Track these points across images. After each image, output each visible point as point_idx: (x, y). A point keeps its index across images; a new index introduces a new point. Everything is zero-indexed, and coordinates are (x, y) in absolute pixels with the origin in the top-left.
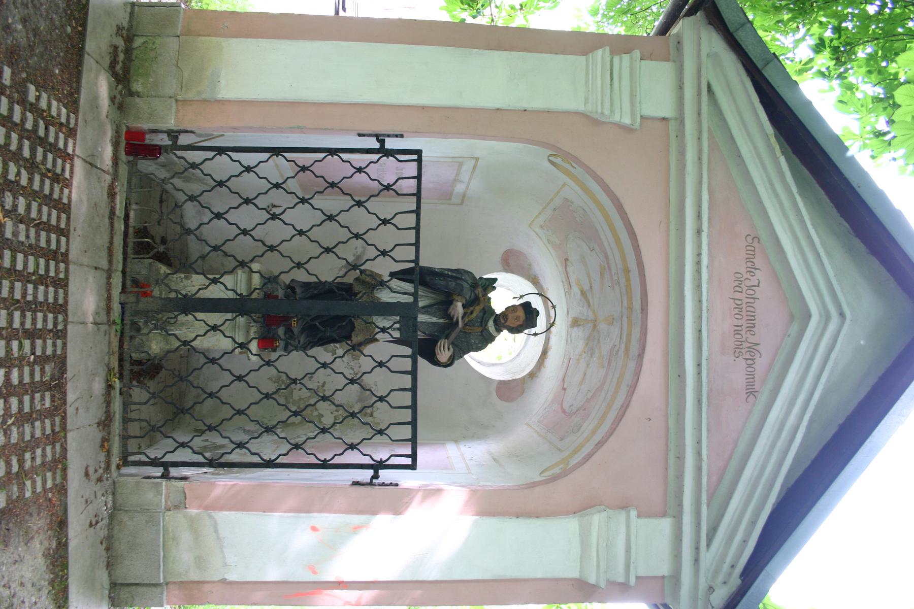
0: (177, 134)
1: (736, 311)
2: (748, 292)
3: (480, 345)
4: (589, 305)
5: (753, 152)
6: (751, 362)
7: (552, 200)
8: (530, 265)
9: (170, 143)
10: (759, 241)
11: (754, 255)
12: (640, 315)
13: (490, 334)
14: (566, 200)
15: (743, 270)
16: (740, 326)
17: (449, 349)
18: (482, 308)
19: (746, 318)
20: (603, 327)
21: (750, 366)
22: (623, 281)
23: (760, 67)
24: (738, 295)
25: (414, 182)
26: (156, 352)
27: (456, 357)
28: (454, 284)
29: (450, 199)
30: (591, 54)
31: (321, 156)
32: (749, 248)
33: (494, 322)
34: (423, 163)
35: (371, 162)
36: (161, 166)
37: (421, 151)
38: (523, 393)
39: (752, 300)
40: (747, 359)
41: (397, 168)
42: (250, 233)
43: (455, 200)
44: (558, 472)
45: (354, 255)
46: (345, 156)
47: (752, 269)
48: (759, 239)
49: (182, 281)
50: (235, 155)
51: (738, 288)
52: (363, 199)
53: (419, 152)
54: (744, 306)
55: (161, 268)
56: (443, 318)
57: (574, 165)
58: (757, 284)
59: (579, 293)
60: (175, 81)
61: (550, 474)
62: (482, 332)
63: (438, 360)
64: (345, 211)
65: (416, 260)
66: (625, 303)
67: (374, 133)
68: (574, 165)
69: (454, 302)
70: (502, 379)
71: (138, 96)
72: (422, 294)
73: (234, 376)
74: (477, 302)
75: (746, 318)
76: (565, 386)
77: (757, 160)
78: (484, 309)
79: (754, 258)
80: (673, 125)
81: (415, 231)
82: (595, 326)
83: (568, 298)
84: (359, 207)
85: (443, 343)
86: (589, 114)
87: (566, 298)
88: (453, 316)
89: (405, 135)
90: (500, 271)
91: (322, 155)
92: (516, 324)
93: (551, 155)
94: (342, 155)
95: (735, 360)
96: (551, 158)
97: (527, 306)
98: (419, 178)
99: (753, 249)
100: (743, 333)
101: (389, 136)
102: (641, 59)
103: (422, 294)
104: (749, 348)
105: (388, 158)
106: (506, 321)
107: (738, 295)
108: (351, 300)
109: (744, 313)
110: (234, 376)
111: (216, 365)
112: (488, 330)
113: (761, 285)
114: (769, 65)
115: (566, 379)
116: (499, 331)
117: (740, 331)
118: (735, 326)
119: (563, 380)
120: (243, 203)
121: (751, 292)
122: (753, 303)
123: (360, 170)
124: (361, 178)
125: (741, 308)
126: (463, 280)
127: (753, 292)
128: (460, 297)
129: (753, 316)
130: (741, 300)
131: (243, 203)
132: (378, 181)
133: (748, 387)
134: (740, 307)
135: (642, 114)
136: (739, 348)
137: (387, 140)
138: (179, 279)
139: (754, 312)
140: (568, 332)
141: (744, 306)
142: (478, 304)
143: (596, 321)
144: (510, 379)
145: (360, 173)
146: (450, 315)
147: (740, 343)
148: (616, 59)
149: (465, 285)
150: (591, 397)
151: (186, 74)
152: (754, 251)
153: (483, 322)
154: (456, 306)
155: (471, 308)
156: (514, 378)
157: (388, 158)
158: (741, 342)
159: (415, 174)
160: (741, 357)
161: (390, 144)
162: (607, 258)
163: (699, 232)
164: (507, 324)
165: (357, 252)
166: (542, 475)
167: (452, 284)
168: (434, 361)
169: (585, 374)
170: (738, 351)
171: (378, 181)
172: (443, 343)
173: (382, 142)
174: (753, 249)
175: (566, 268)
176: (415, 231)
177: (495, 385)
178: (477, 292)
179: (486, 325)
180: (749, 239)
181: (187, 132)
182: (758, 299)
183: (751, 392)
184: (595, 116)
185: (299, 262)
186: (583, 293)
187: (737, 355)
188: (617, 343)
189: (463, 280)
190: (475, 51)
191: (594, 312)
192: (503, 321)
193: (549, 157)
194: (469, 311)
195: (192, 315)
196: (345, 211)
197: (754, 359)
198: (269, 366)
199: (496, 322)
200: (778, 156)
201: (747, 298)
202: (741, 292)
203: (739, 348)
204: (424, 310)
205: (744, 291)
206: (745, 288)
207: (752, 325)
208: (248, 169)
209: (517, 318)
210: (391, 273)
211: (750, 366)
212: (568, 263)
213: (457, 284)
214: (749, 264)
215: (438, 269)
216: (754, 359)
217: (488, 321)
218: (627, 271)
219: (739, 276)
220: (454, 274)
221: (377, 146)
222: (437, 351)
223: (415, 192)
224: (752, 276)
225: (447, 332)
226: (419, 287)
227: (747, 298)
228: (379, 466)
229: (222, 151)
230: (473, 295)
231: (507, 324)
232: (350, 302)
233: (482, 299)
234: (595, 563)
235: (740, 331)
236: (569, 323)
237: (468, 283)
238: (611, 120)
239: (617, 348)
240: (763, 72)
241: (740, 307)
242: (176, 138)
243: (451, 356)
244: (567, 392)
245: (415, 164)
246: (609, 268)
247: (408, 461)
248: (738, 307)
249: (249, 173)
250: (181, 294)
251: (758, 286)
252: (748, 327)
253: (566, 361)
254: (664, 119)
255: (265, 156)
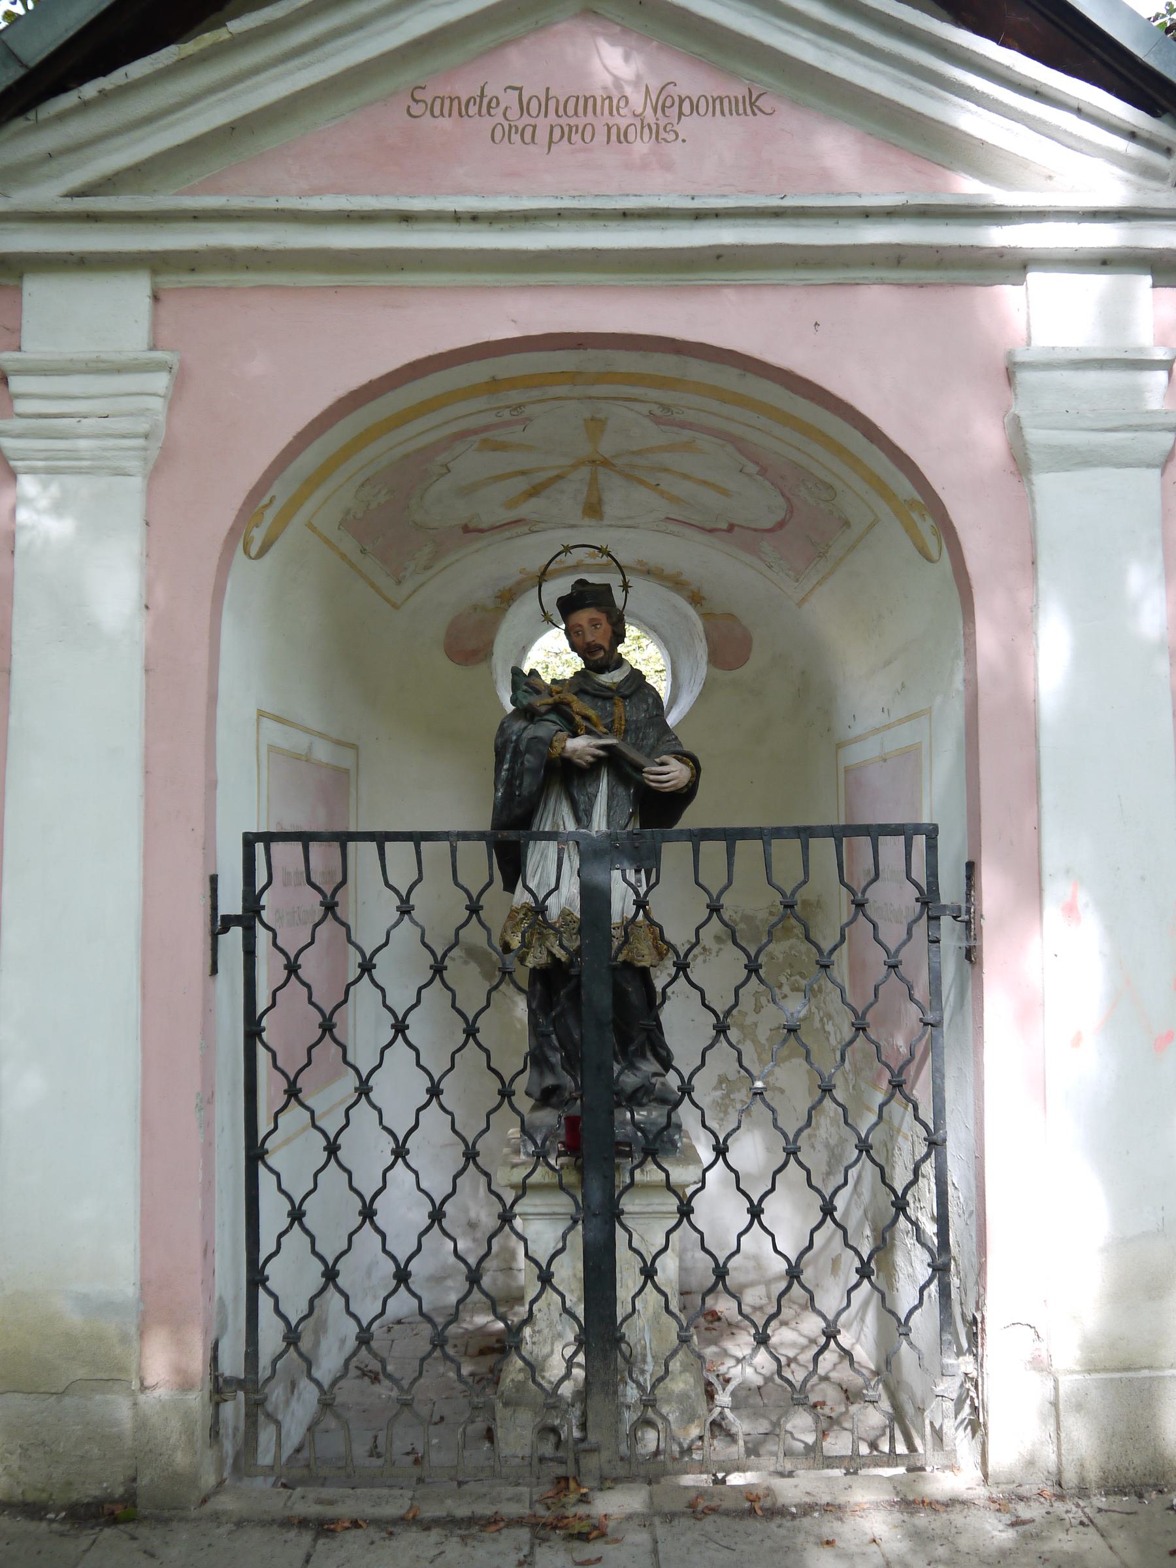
0: (221, 1380)
1: (576, 138)
2: (534, 112)
3: (650, 701)
4: (559, 477)
5: (221, 95)
6: (686, 105)
7: (343, 556)
8: (475, 608)
9: (241, 1395)
10: (421, 88)
11: (452, 100)
12: (591, 353)
13: (627, 679)
14: (343, 523)
15: (487, 123)
16: (609, 129)
17: (662, 764)
18: (575, 698)
19: (590, 117)
20: (607, 447)
21: (694, 108)
22: (515, 397)
23: (21, 72)
24: (542, 135)
25: (314, 847)
26: (692, 1380)
27: (678, 748)
28: (527, 756)
29: (347, 771)
30: (12, 463)
31: (262, 1055)
32: (437, 111)
33: (602, 672)
34: (273, 829)
35: (275, 944)
36: (292, 1392)
37: (246, 836)
38: (731, 616)
39: (552, 104)
40: (681, 114)
41: (285, 885)
42: (438, 1203)
43: (346, 760)
44: (930, 521)
45: (466, 963)
46: (262, 1002)
47: (484, 103)
48: (416, 88)
49: (539, 1332)
50: (267, 1246)
51: (528, 135)
52: (355, 958)
53: (249, 841)
54: (564, 121)
55: (513, 1380)
56: (598, 778)
57: (266, 500)
58: (517, 92)
59: (534, 500)
60: (98, 1397)
61: (934, 538)
62: (624, 697)
63: (687, 786)
64: (384, 997)
65: (480, 836)
66: (561, 390)
67: (209, 939)
68: (266, 500)
69: (567, 755)
70: (705, 658)
71: (134, 1480)
72: (549, 823)
73: (751, 1224)
74: (565, 708)
75: (590, 117)
76: (725, 526)
77: (240, 87)
78: (576, 694)
79: (458, 98)
80: (168, 281)
81: (423, 843)
82: (606, 463)
83: (542, 525)
84: (374, 966)
85: (652, 777)
86: (150, 466)
87: (544, 530)
88: (594, 756)
89: (212, 872)
90: (490, 667)
91: (261, 1051)
92: (605, 627)
93: (246, 551)
94: (260, 1008)
95: (684, 141)
96: (254, 550)
97: (568, 606)
98: (305, 838)
99: (438, 102)
100: (623, 123)
101: (214, 908)
102: (19, 349)
103: (549, 823)
104: (655, 111)
105: (263, 908)
106: (601, 648)
107: (542, 135)
108: (579, 976)
109: (580, 121)
110: (751, 1224)
111: (730, 1265)
112: (620, 685)
113: (518, 85)
114: (18, 50)
115: (709, 526)
116: (620, 662)
117: (619, 129)
118: (608, 141)
119: (711, 531)
120: (372, 1223)
121: (534, 104)
122: (558, 101)
123: (292, 968)
124: (309, 966)
125: (570, 128)
126: (519, 737)
127: (534, 101)
128: (556, 744)
129: (586, 100)
130: (552, 127)
131: (372, 1223)
132: (316, 926)
133: (741, 111)
134: (566, 130)
135: (146, 346)
136: (657, 132)
137: (223, 911)
138: (535, 1339)
139: (578, 98)
140: (611, 526)
141: (564, 121)
142: (568, 705)
143: (594, 461)
144: (704, 641)
145: (299, 967)
146: (591, 764)
147: (646, 130)
148: (21, 406)
149: (528, 734)
150: (757, 463)
151: (81, 1373)
152: (443, 99)
153: (604, 695)
154: (575, 751)
155: (578, 718)
156: (702, 635)
157: (263, 908)
158: (642, 128)
159: (298, 847)
160: (676, 128)
161: (231, 902)
162: (463, 435)
163: (406, 218)
164: (606, 645)
165: (461, 957)
166: (934, 553)
167: (529, 760)
168: (684, 796)
169: (705, 483)
170: (662, 134)
171: (316, 926)
172: (652, 777)
173: (229, 922)
174: (438, 102)
175: (482, 531)
176: (423, 843)
177: (719, 673)
178: (543, 709)
179: (608, 688)
180: (417, 109)
181: (215, 1359)
182: (548, 89)
183: (752, 104)
184: (154, 453)
185: (500, 1092)
186: (535, 492)
187: (672, 136)
188: (644, 408)
189: (519, 737)
190: (13, 721)
191: (575, 467)
192: (601, 654)
193: (250, 558)
194: (585, 723)
195: (621, 1324)
196: (384, 997)
197: (680, 97)
198: (727, 1149)
199: (603, 668)
200: (228, 36)
201: (546, 116)
202: (535, 127)
203: (657, 132)
204: (584, 818)
205: (532, 121)
206: (526, 119)
207: (607, 102)
208: (297, 1215)
209: (594, 623)
210: (505, 889)
211: (694, 108)
212: (472, 525)
213: (528, 750)
214: (473, 110)
215: (496, 790)
216: (680, 97)
217: (600, 685)
218: (494, 385)
219: (499, 130)
220: (508, 756)
221: (237, 932)
222: (668, 787)
223: (336, 845)
224: (498, 104)
225: (629, 769)
226: (534, 829)
227: (546, 116)
228: (928, 899)
229: (256, 1278)
230: (553, 717)
231: (606, 645)
232: (583, 979)
233: (556, 697)
234: (1130, 435)
235: (619, 129)
236: (593, 522)
237: (525, 728)
238: (162, 418)
239: (658, 411)
240: (32, 64)
241: (566, 130)
242: (229, 1381)
243: (679, 760)
244: (735, 522)
245: (275, 847)
246: (486, 428)
247: (920, 841)
248: (568, 133)
249: (304, 1214)
250: (575, 1354)
251: (520, 89)
252: (611, 113)
253: (673, 527)
254: (156, 298)
255: (266, 1180)
